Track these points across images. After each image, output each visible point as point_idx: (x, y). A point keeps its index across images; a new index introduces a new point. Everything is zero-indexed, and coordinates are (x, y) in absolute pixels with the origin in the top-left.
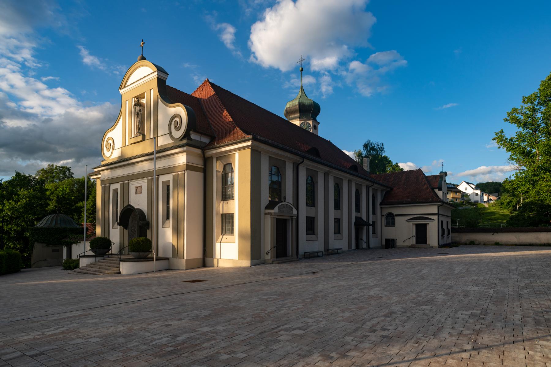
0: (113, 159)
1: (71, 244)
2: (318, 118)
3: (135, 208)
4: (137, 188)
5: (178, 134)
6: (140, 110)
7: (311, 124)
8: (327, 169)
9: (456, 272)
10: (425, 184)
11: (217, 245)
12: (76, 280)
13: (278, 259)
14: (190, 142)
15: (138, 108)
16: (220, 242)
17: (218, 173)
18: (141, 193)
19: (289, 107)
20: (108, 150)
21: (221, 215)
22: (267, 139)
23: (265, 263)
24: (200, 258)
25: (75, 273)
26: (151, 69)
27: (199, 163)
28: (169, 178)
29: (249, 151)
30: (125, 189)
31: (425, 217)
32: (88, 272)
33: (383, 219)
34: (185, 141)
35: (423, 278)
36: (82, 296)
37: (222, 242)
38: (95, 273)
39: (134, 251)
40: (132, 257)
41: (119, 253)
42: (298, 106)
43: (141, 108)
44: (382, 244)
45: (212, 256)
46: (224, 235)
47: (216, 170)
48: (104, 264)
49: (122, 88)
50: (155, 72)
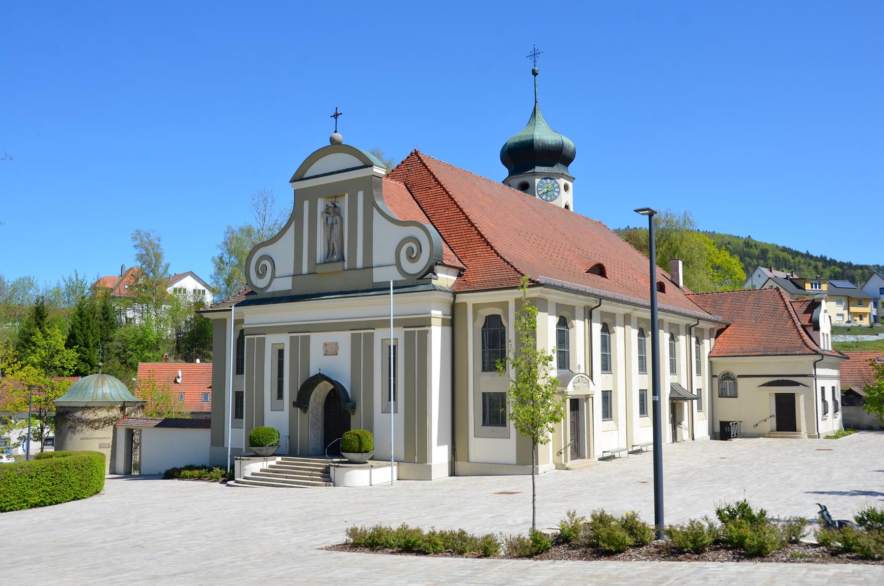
9: (834, 478)
18: (337, 354)
30: (302, 348)
33: (716, 380)
35: (792, 485)
44: (715, 431)
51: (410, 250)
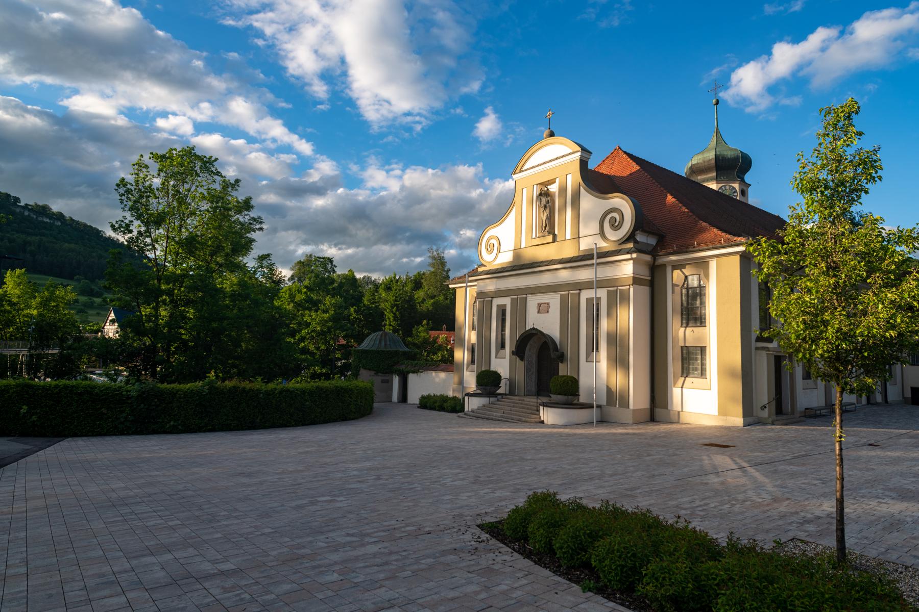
0: (499, 264)
1: (408, 373)
2: (748, 178)
4: (539, 305)
6: (548, 202)
7: (737, 189)
11: (676, 392)
15: (544, 200)
16: (681, 386)
18: (548, 312)
19: (698, 164)
20: (490, 252)
21: (680, 348)
24: (647, 408)
26: (566, 147)
27: (645, 274)
30: (520, 308)
34: (630, 245)
37: (684, 387)
42: (713, 162)
43: (549, 198)
44: (905, 396)
46: (687, 376)
47: (672, 283)
49: (516, 172)
50: (577, 152)
51: (613, 220)
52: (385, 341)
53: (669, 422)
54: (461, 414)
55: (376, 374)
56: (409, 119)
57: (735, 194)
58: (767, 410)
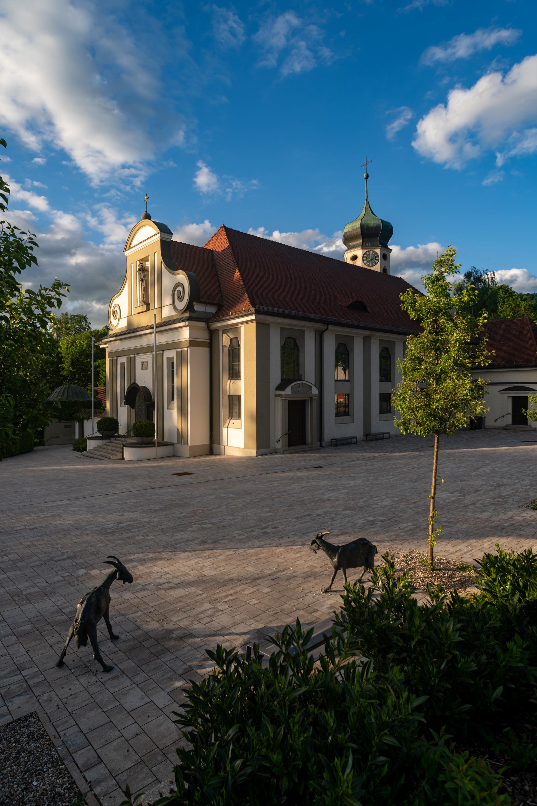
3: (140, 385)
4: (143, 363)
5: (182, 305)
8: (366, 333)
10: (531, 338)
11: (224, 430)
12: (79, 467)
13: (291, 448)
14: (193, 315)
17: (225, 348)
19: (348, 232)
22: (276, 309)
23: (275, 452)
25: (82, 457)
27: (204, 336)
28: (172, 354)
29: (254, 324)
30: (132, 362)
31: (526, 387)
32: (94, 456)
34: (187, 315)
36: (75, 487)
38: (99, 457)
39: (137, 436)
40: (136, 442)
41: (126, 434)
42: (359, 230)
45: (219, 442)
48: (110, 448)
50: (158, 233)
52: (68, 393)
53: (220, 454)
54: (84, 453)
55: (60, 421)
56: (127, 172)
57: (377, 258)
58: (280, 443)
